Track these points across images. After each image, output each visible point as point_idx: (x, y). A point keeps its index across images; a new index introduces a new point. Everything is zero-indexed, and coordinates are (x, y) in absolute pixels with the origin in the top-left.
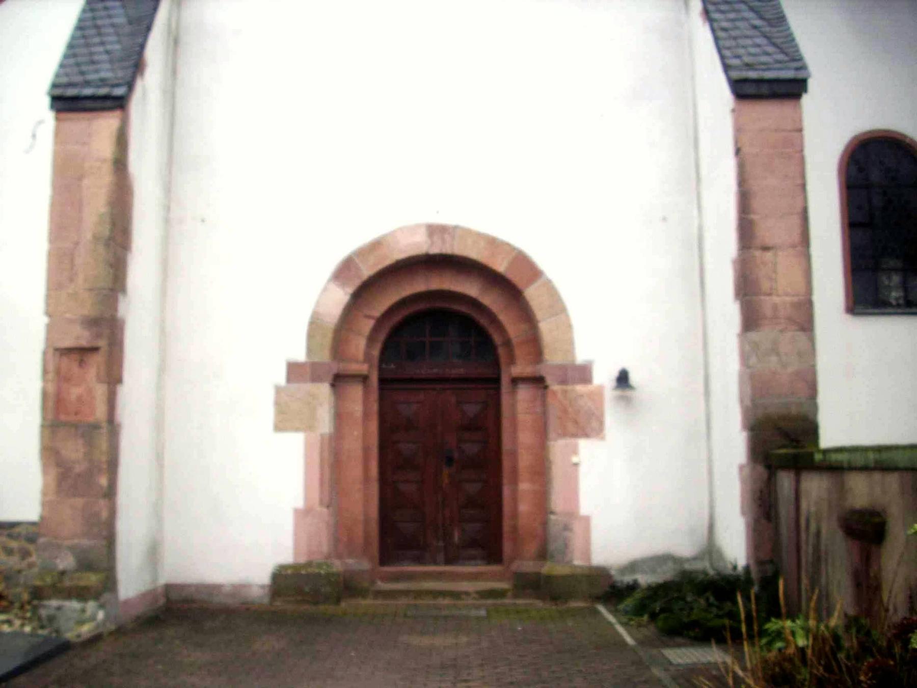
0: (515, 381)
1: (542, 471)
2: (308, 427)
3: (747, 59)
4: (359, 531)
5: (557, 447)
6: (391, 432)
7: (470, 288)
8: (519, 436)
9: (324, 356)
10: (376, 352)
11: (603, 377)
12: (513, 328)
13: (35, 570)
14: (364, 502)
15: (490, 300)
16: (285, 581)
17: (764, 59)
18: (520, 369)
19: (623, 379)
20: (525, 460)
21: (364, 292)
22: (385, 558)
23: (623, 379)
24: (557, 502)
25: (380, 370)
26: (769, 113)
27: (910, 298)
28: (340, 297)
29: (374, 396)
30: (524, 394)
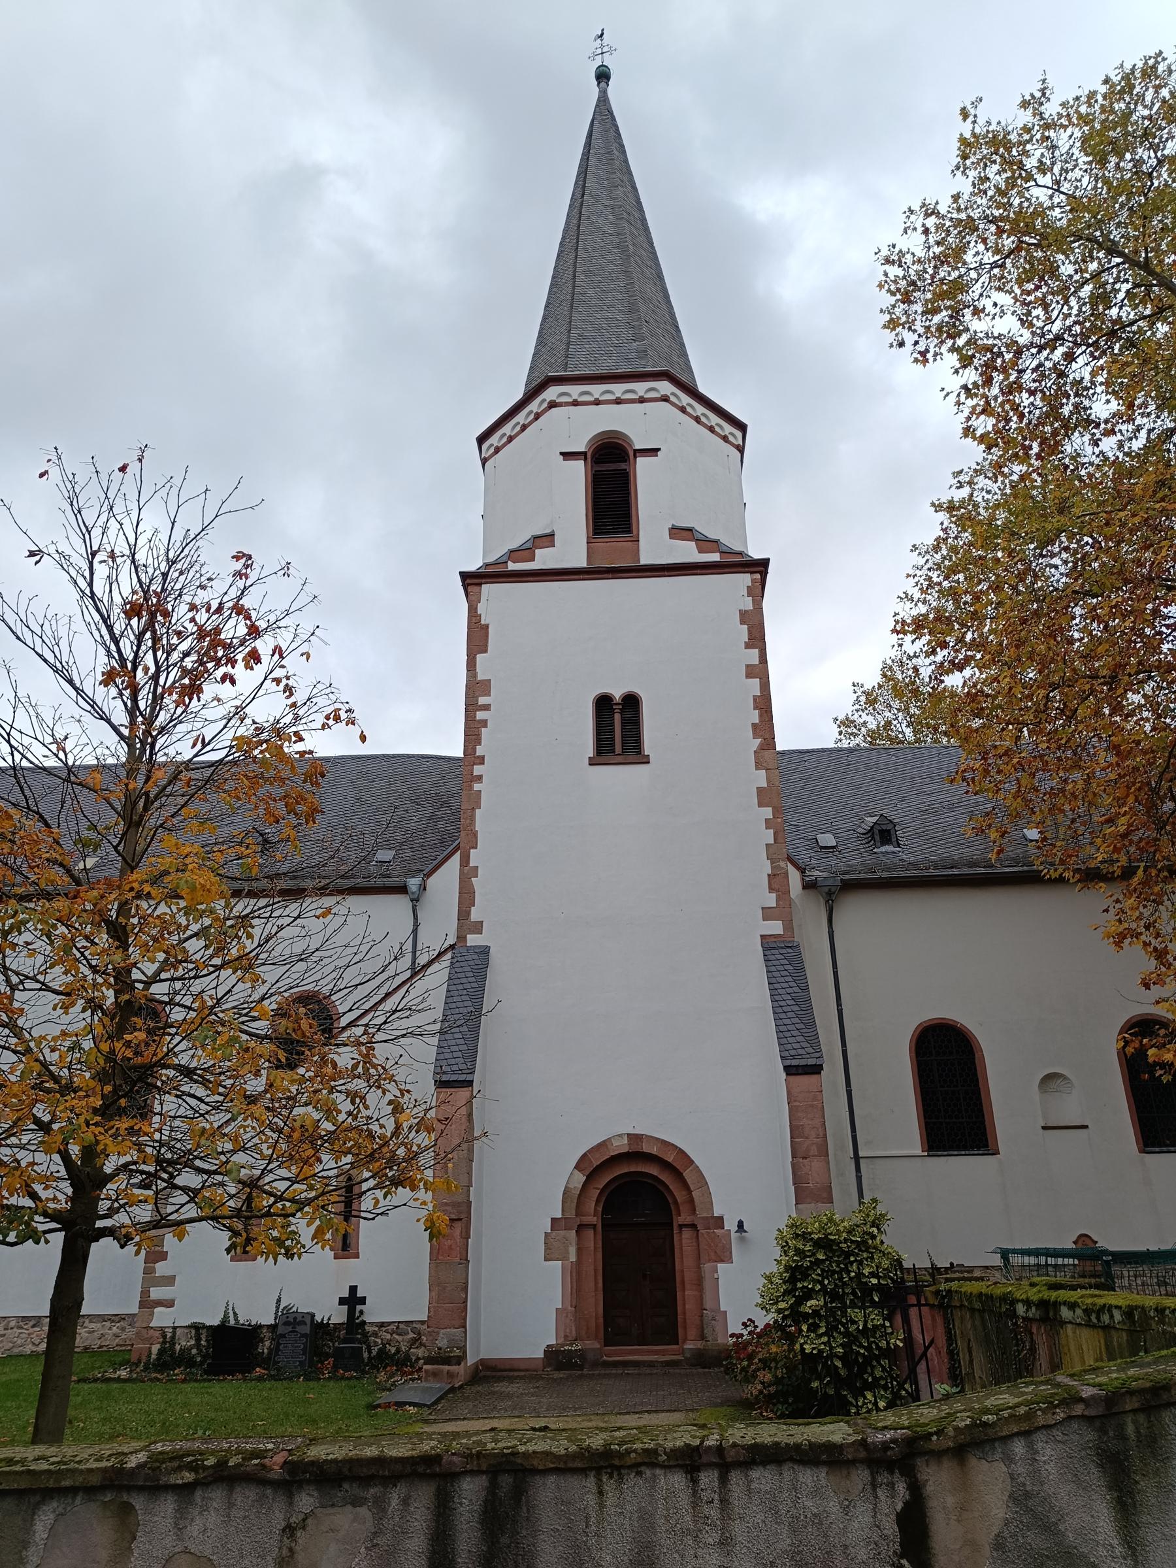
0: (681, 1226)
1: (699, 1283)
2: (564, 1258)
3: (793, 1052)
4: (593, 1324)
5: (707, 1267)
6: (610, 1253)
7: (654, 1171)
8: (684, 1261)
9: (571, 1214)
10: (600, 1209)
11: (730, 1225)
12: (680, 1196)
13: (300, 747)
14: (595, 1305)
15: (665, 1177)
16: (550, 1352)
17: (801, 1051)
18: (684, 1218)
19: (740, 1225)
20: (689, 1276)
21: (590, 1178)
22: (607, 1343)
23: (740, 1225)
24: (708, 1304)
25: (603, 1219)
26: (804, 1082)
27: (546, 1490)
28: (580, 1178)
29: (600, 1237)
30: (687, 1234)
